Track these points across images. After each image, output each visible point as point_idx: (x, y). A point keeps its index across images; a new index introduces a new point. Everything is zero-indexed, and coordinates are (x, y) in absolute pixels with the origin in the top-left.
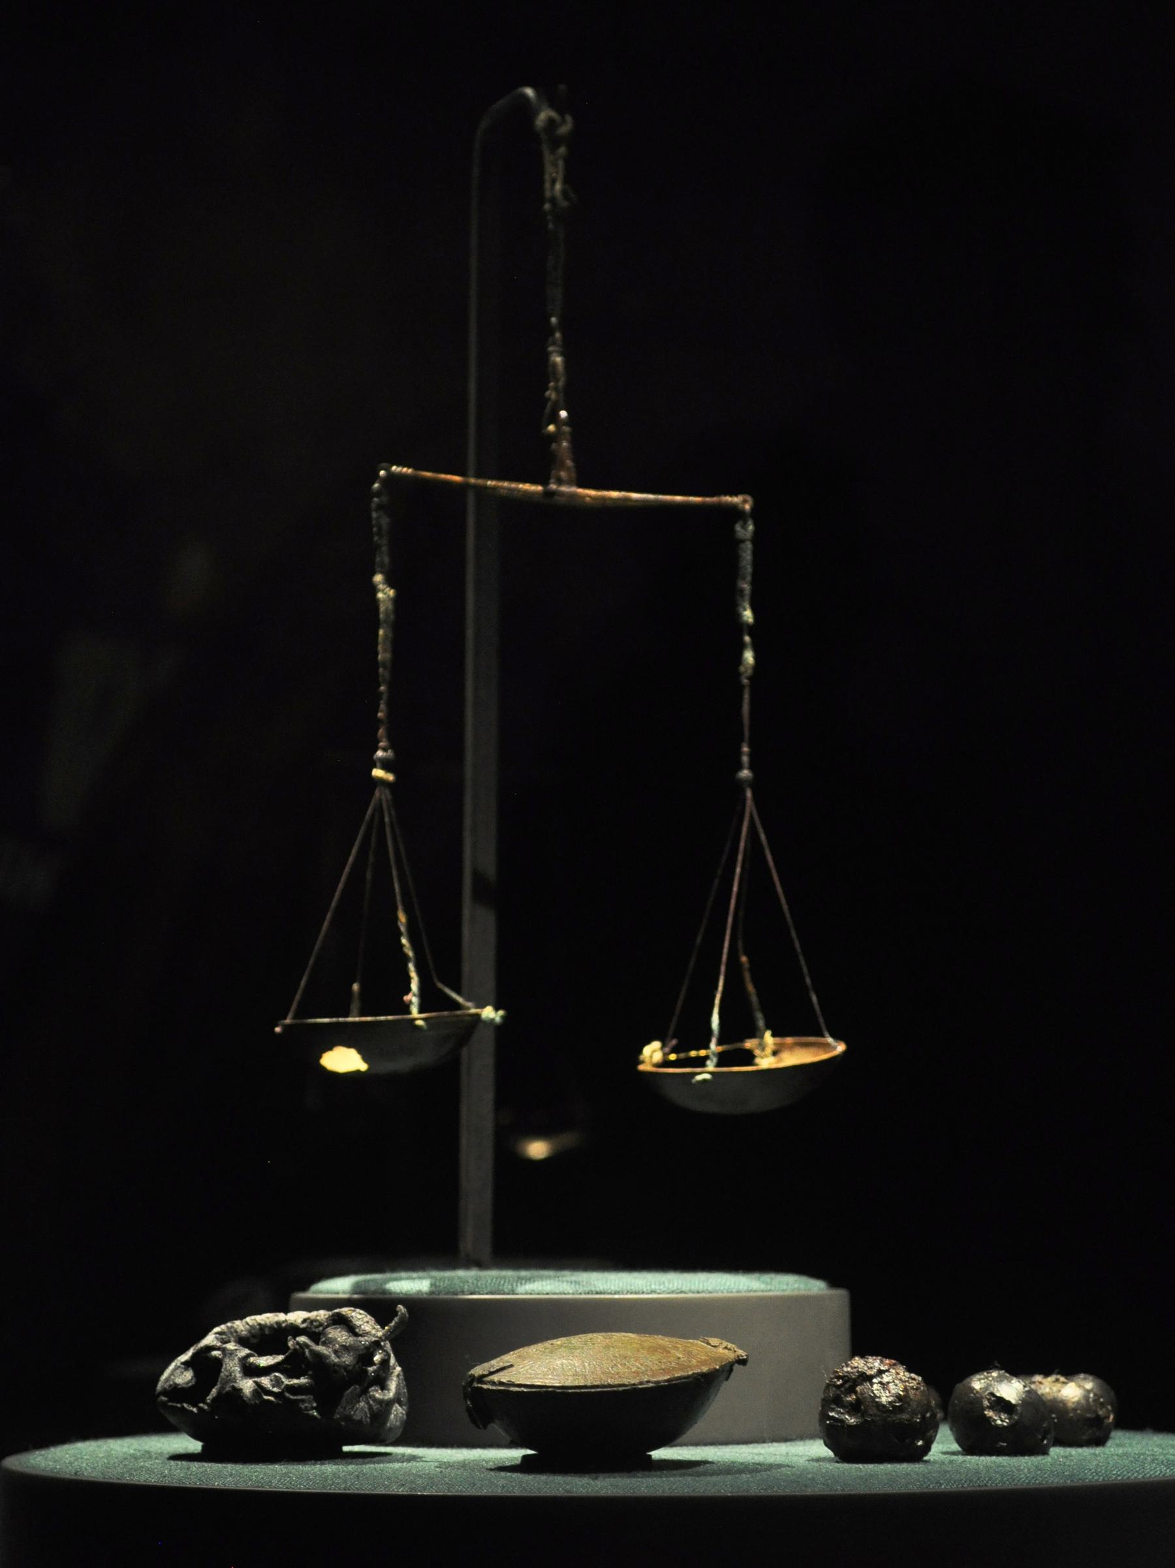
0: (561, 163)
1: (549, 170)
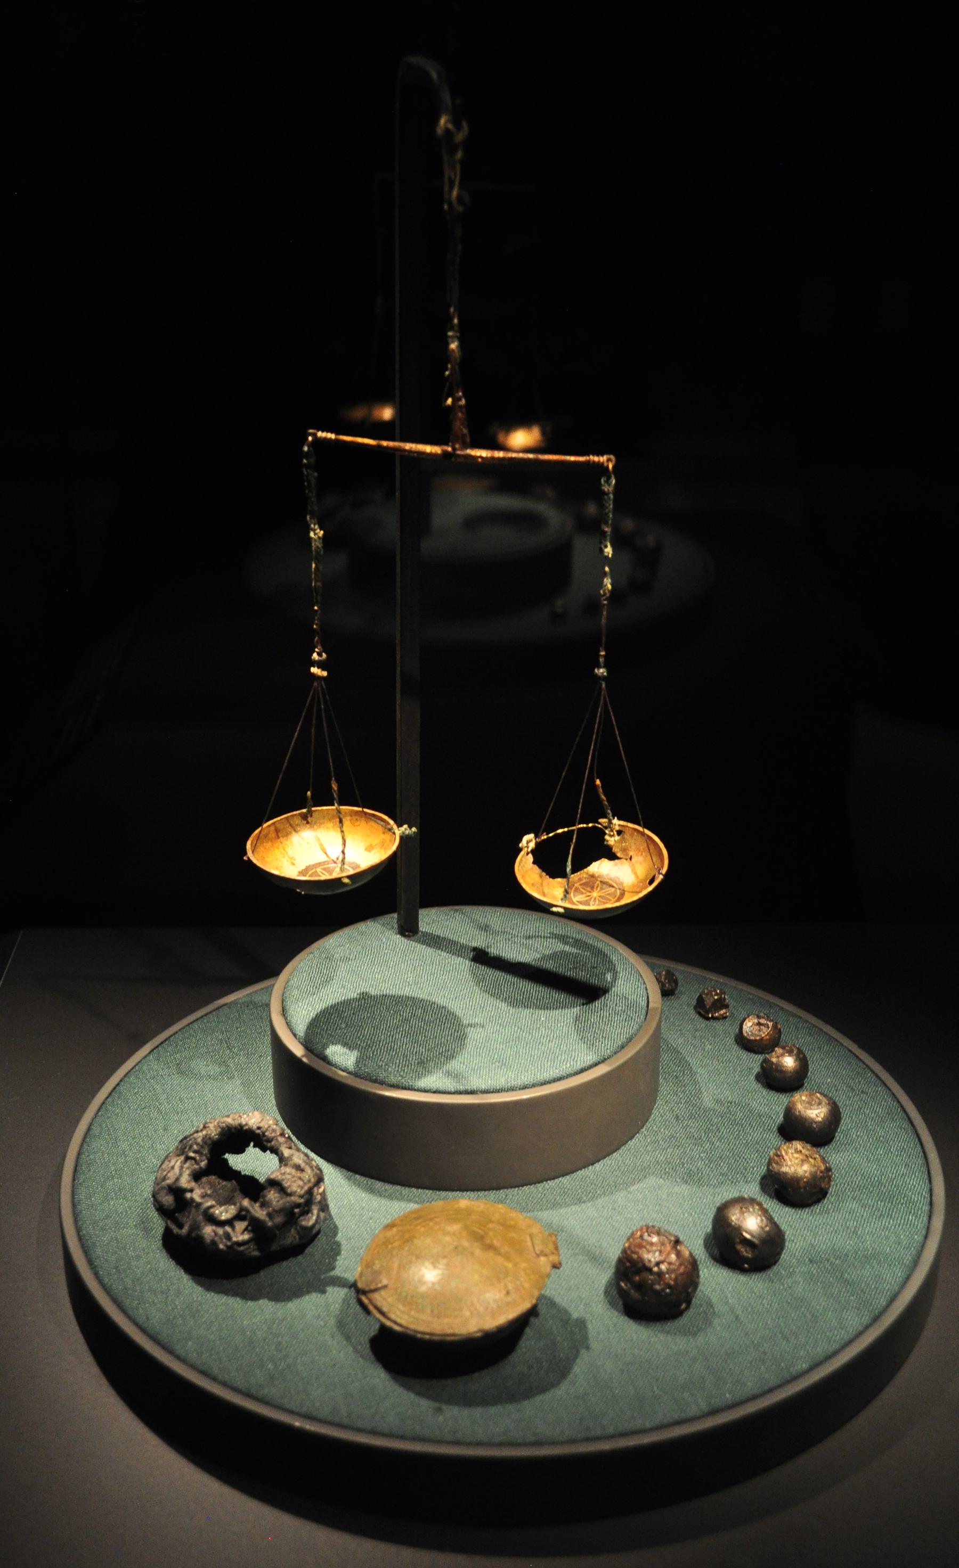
0: (458, 167)
1: (447, 172)
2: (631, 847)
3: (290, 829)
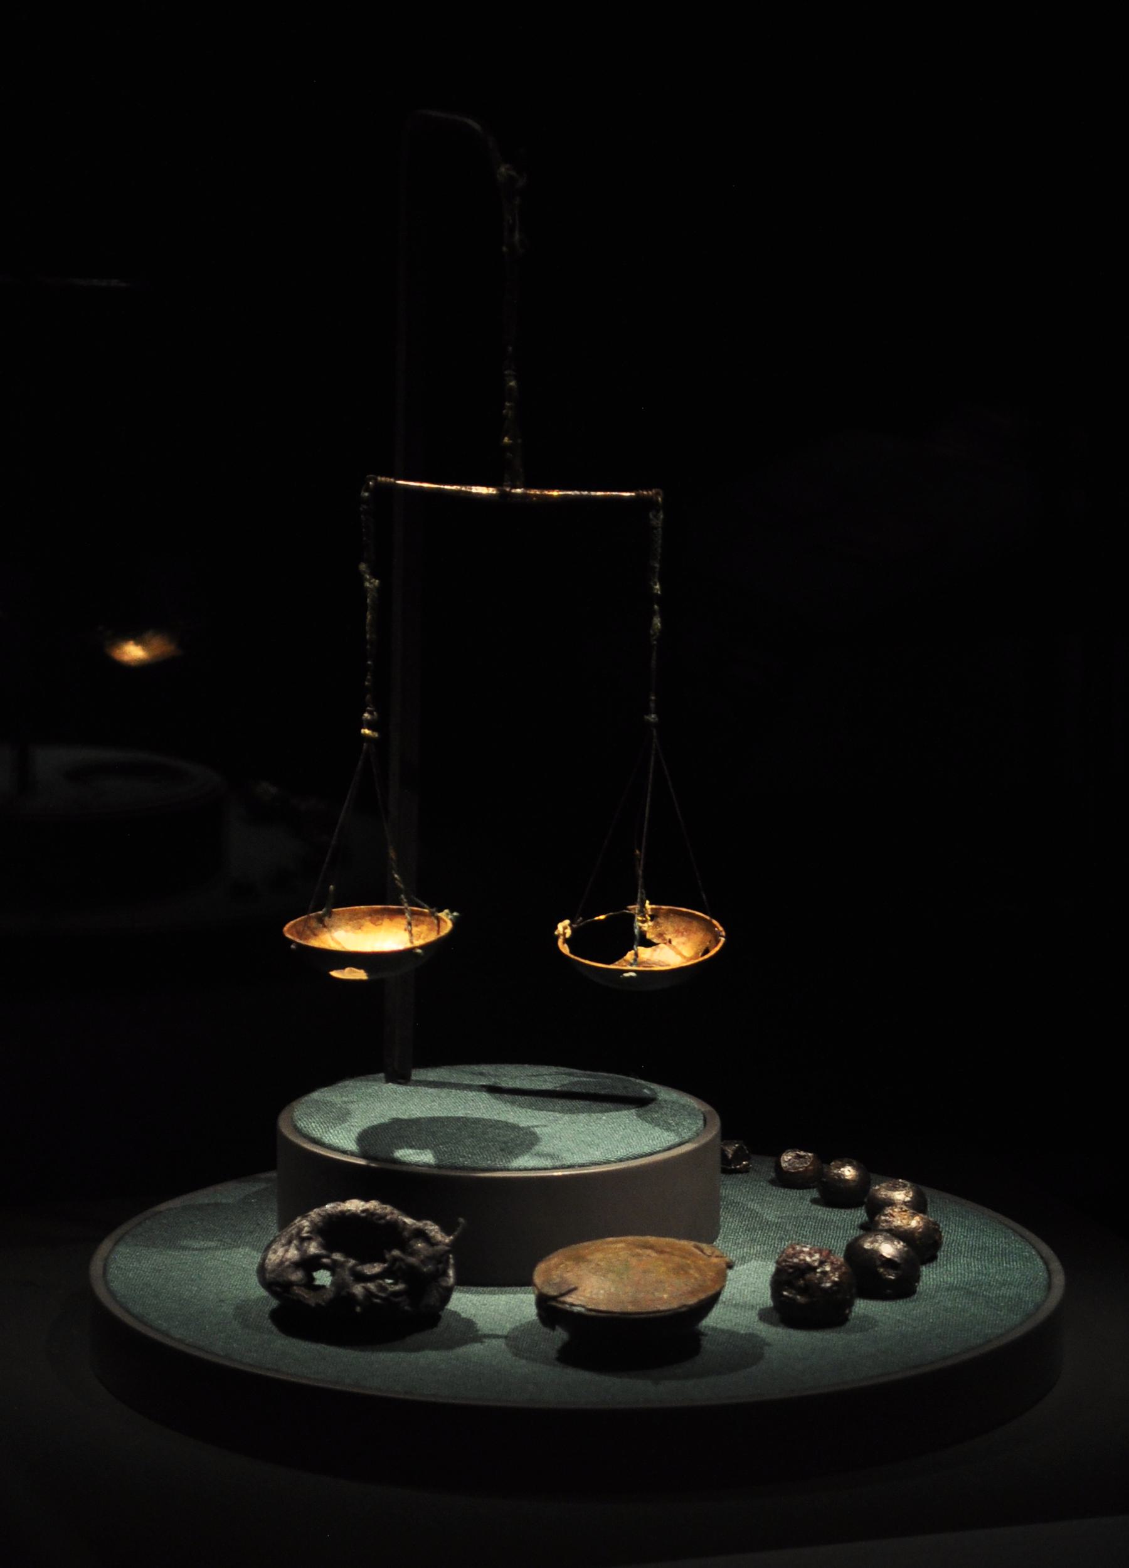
2: (667, 930)
3: (308, 932)
